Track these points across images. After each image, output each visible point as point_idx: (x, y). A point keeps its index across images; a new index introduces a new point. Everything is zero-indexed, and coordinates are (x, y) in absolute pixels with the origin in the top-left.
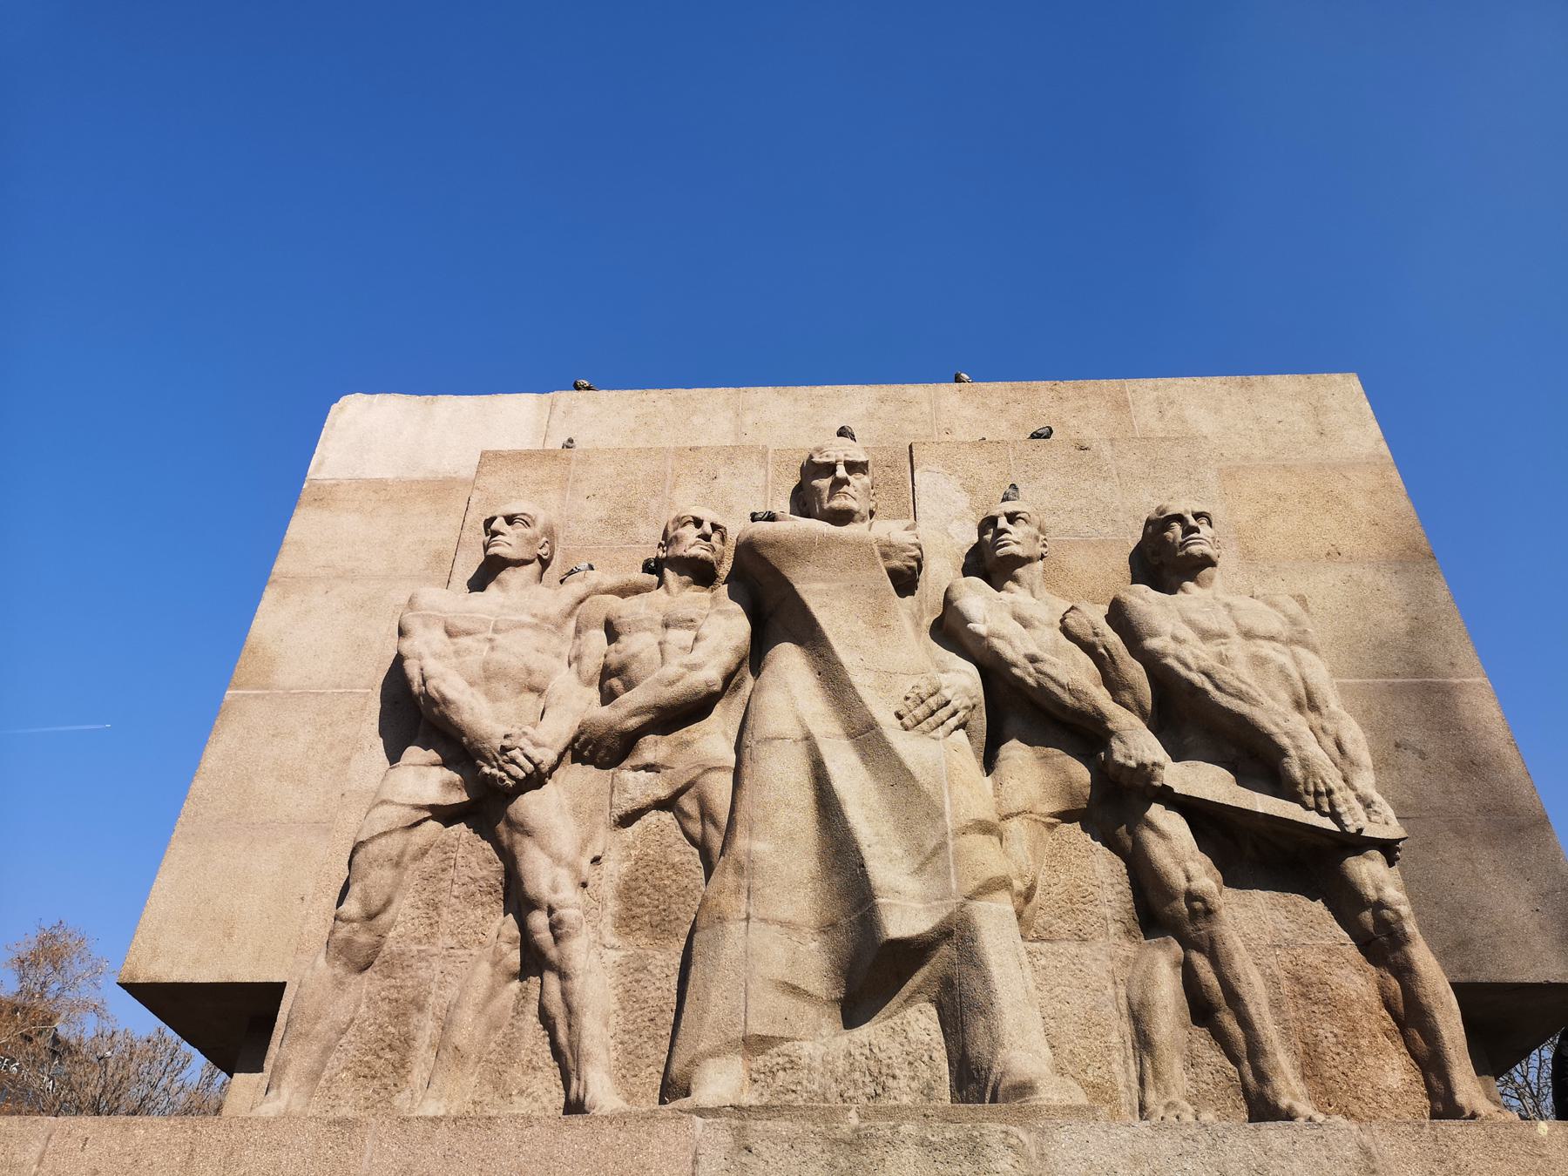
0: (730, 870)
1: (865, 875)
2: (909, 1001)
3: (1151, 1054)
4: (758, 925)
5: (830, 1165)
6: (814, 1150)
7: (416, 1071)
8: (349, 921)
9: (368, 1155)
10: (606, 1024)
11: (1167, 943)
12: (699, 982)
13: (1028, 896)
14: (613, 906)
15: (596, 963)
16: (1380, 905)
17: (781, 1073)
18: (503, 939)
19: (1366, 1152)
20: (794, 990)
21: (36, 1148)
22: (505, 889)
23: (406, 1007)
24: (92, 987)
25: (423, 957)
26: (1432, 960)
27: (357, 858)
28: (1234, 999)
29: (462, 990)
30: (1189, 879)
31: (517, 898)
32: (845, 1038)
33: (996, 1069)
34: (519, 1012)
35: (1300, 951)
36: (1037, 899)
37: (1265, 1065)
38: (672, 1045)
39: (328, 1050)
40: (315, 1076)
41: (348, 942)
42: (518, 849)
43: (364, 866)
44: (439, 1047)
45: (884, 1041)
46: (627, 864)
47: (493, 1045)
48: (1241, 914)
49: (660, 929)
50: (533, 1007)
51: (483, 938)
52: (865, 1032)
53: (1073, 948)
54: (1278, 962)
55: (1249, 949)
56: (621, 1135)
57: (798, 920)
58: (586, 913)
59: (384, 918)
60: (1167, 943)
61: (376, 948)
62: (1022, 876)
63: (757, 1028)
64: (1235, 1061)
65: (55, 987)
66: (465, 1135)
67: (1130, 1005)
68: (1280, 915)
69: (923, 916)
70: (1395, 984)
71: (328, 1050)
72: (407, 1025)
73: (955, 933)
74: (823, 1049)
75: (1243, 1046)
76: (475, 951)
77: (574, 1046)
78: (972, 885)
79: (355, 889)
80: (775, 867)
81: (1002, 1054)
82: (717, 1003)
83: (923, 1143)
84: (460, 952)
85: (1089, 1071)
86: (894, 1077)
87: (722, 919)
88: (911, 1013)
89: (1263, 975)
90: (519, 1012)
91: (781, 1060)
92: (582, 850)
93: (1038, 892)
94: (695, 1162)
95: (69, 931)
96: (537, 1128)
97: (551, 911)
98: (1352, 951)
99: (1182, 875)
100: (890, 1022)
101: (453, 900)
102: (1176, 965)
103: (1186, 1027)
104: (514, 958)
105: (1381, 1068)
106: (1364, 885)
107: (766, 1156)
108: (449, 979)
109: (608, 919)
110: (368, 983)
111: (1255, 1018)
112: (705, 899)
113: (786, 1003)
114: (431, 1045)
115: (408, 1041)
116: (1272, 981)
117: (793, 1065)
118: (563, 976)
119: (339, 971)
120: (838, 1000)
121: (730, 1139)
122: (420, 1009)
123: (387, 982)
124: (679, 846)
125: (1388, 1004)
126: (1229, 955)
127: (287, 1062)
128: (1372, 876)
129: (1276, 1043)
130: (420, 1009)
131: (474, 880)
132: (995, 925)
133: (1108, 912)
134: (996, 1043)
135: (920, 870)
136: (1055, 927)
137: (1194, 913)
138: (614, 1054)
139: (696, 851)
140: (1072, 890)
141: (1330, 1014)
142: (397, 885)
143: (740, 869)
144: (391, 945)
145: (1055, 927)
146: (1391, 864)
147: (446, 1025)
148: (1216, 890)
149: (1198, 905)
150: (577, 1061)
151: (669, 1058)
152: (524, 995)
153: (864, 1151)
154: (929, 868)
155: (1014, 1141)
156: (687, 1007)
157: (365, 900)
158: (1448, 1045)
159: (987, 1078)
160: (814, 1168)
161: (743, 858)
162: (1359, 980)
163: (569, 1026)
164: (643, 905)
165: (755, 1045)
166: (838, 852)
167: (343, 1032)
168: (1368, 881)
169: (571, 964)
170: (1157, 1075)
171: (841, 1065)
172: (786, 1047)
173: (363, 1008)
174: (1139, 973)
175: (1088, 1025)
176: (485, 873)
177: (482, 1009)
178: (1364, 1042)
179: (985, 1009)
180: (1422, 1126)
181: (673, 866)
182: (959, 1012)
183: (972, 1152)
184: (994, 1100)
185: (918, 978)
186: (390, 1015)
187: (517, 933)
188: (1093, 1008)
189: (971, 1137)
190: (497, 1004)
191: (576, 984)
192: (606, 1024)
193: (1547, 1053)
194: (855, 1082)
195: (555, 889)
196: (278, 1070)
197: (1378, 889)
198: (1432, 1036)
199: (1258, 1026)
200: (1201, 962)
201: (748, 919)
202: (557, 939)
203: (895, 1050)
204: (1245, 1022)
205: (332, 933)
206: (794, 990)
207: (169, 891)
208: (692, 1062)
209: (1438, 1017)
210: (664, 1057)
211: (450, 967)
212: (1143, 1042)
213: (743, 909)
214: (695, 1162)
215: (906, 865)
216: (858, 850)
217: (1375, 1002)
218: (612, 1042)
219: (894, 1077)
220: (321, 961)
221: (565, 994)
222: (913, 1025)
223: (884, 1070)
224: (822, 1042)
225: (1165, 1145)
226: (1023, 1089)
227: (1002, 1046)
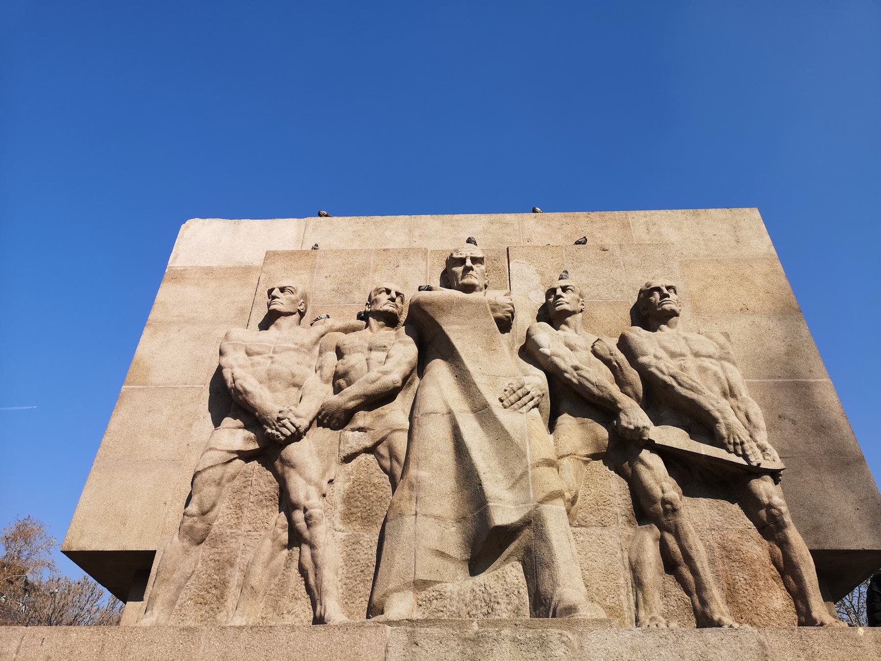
0: (406, 487)
1: (482, 490)
2: (506, 560)
3: (642, 590)
4: (421, 518)
5: (462, 653)
6: (453, 644)
7: (229, 601)
8: (192, 516)
9: (202, 648)
10: (337, 574)
11: (651, 528)
13: (573, 501)
14: (340, 507)
15: (331, 539)
16: (770, 506)
17: (435, 601)
18: (278, 526)
19: (762, 645)
20: (442, 554)
23: (224, 564)
25: (234, 536)
26: (799, 537)
27: (196, 480)
28: (689, 559)
29: (255, 555)
30: (663, 492)
31: (286, 503)
33: (555, 599)
34: (287, 567)
35: (725, 532)
36: (578, 503)
39: (180, 588)
40: (172, 603)
41: (191, 528)
42: (287, 475)
43: (200, 485)
44: (243, 587)
45: (492, 583)
46: (348, 484)
47: (273, 585)
48: (692, 511)
49: (367, 520)
50: (296, 564)
51: (267, 526)
52: (482, 578)
53: (598, 531)
54: (713, 539)
55: (697, 531)
56: (345, 636)
59: (212, 515)
61: (207, 531)
62: (570, 490)
63: (422, 575)
64: (689, 593)
65: (26, 553)
66: (257, 636)
68: (714, 512)
70: (778, 550)
71: (180, 588)
73: (532, 523)
76: (263, 533)
78: (541, 496)
79: (195, 498)
80: (431, 485)
81: (559, 590)
82: (400, 562)
83: (514, 640)
84: (254, 533)
85: (608, 599)
86: (498, 603)
87: (401, 515)
88: (508, 567)
89: (705, 545)
90: (287, 567)
91: (434, 594)
92: (323, 476)
93: (579, 499)
94: (387, 651)
96: (297, 632)
97: (305, 510)
98: (754, 532)
100: (496, 573)
101: (250, 504)
102: (656, 540)
103: (661, 574)
104: (285, 536)
107: (426, 647)
108: (248, 548)
110: (202, 551)
111: (700, 570)
112: (392, 503)
113: (438, 562)
114: (238, 586)
115: (225, 583)
116: (710, 549)
117: (441, 596)
118: (312, 547)
120: (466, 560)
121: (406, 638)
122: (232, 565)
123: (213, 550)
124: (377, 474)
125: (774, 562)
126: (686, 534)
127: (156, 595)
128: (766, 490)
129: (712, 584)
130: (232, 565)
131: (262, 493)
132: (555, 519)
133: (618, 510)
134: (555, 584)
137: (666, 511)
138: (341, 591)
140: (598, 498)
142: (219, 495)
143: (411, 486)
144: (215, 529)
146: (776, 483)
147: (246, 574)
148: (678, 498)
149: (668, 506)
152: (290, 558)
153: (481, 645)
155: (565, 639)
156: (382, 564)
157: (201, 504)
158: (808, 584)
159: (550, 604)
160: (453, 654)
161: (414, 481)
162: (759, 549)
163: (316, 575)
164: (357, 507)
165: (420, 585)
166: (467, 477)
167: (188, 578)
168: (764, 493)
169: (317, 540)
170: (645, 601)
174: (636, 544)
175: (607, 574)
176: (268, 489)
177: (267, 565)
178: (761, 583)
179: (549, 565)
180: (793, 630)
181: (374, 485)
182: (535, 567)
183: (542, 645)
184: (554, 616)
185: (512, 548)
186: (215, 569)
188: (610, 564)
189: (541, 637)
190: (275, 562)
191: (320, 551)
193: (864, 589)
194: (476, 606)
195: (307, 498)
196: (152, 600)
197: (769, 497)
198: (799, 579)
199: (702, 574)
200: (670, 538)
201: (416, 514)
202: (309, 526)
203: (499, 588)
204: (695, 572)
205: (182, 522)
206: (442, 554)
209: (803, 569)
210: (369, 592)
211: (248, 542)
212: (638, 583)
213: (413, 508)
214: (387, 651)
215: (505, 484)
216: (478, 476)
217: (767, 560)
219: (498, 603)
220: (176, 538)
221: (313, 557)
222: (509, 574)
223: (493, 599)
224: (458, 584)
225: (650, 641)
226: (570, 610)
227: (559, 585)
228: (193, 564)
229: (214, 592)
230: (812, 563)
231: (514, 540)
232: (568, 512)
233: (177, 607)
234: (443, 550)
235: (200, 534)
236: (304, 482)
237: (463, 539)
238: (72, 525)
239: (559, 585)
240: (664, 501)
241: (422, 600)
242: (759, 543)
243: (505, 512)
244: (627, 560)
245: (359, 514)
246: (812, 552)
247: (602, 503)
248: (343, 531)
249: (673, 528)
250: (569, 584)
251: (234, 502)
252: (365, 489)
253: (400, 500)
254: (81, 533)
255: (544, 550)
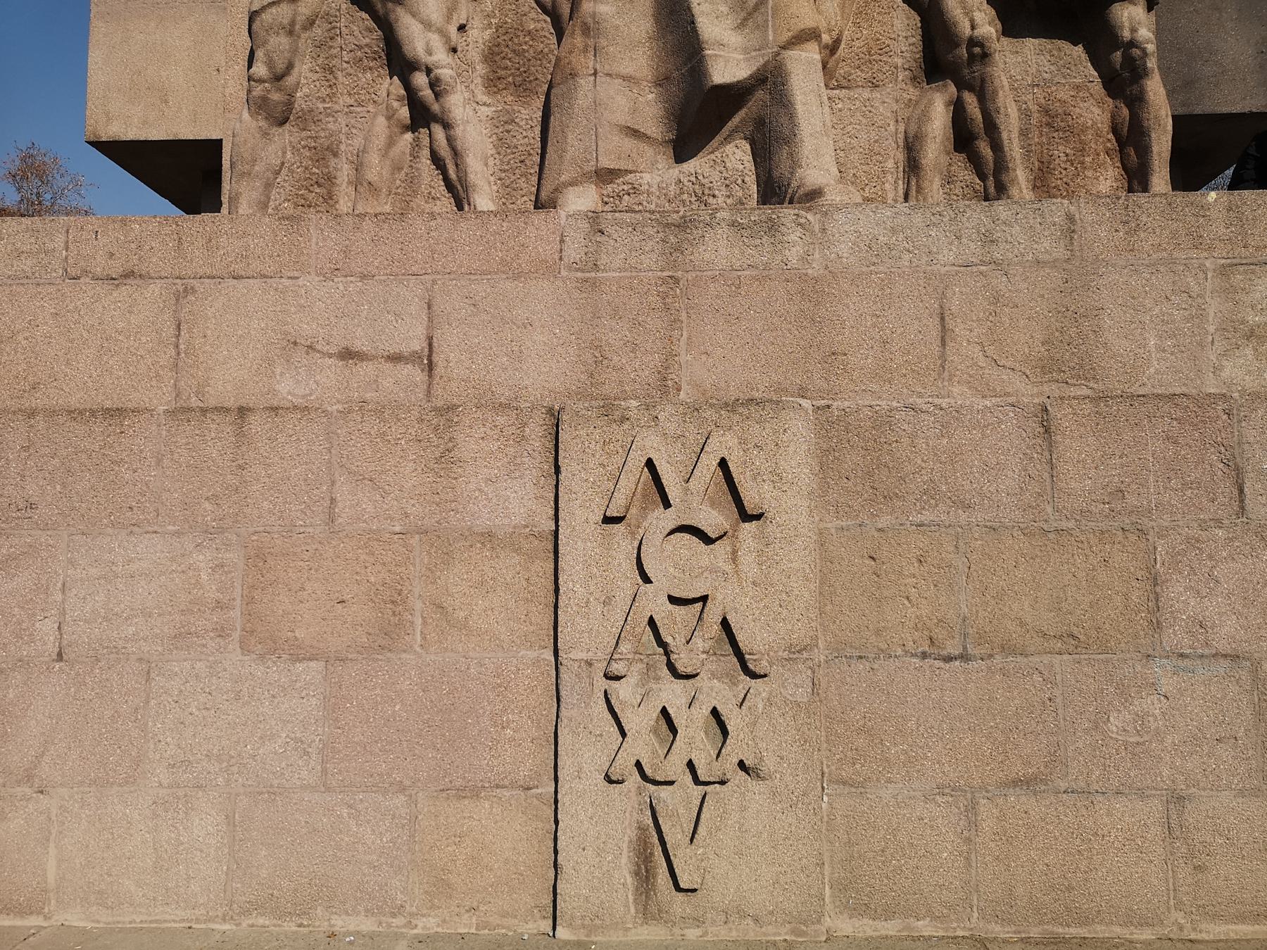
0: (578, 32)
1: (695, 31)
2: (728, 139)
3: (918, 176)
4: (603, 79)
6: (651, 231)
7: (341, 202)
8: (261, 81)
10: (486, 165)
11: (945, 86)
13: (833, 48)
14: (481, 69)
15: (472, 115)
16: (1132, 44)
17: (626, 197)
18: (392, 97)
19: (1070, 218)
20: (635, 133)
23: (325, 153)
25: (330, 113)
26: (1162, 91)
27: (254, 27)
28: (991, 128)
29: (366, 139)
30: (973, 28)
31: (399, 62)
33: (794, 184)
34: (415, 157)
35: (1054, 88)
36: (841, 52)
39: (268, 186)
40: (264, 206)
41: (264, 99)
42: (392, 17)
43: (263, 33)
44: (357, 183)
45: (707, 171)
46: (488, 32)
47: (398, 182)
48: (1011, 59)
49: (522, 88)
50: (426, 152)
51: (376, 98)
52: (691, 165)
53: (866, 94)
54: (1032, 100)
55: (1013, 89)
59: (290, 80)
61: (289, 105)
62: (830, 31)
63: (606, 162)
64: (982, 176)
65: (48, 196)
68: (1043, 60)
70: (1125, 112)
71: (268, 186)
73: (770, 80)
76: (371, 108)
78: (786, 36)
79: (260, 54)
80: (617, 27)
81: (799, 172)
82: (574, 146)
83: (733, 224)
84: (359, 109)
85: (867, 189)
86: (714, 196)
87: (573, 75)
88: (729, 148)
89: (1019, 110)
90: (415, 157)
91: (626, 187)
92: (449, 18)
93: (843, 46)
94: (562, 241)
96: (439, 220)
97: (429, 71)
98: (1097, 87)
100: (712, 156)
101: (345, 65)
102: (948, 104)
103: (948, 154)
104: (404, 112)
108: (354, 131)
110: (286, 136)
111: (1006, 142)
112: (558, 59)
113: (629, 143)
114: (350, 183)
115: (330, 179)
116: (1025, 114)
117: (635, 190)
118: (447, 126)
120: (671, 141)
121: (587, 225)
122: (335, 155)
123: (304, 134)
124: (533, 15)
125: (1115, 130)
126: (995, 92)
127: (238, 195)
128: (1130, 19)
129: (1018, 162)
130: (335, 155)
131: (360, 47)
132: (803, 72)
133: (899, 61)
134: (795, 164)
137: (972, 57)
138: (495, 188)
140: (872, 43)
142: (294, 51)
143: (586, 31)
144: (300, 103)
146: (1150, 9)
147: (358, 167)
148: (994, 35)
149: (977, 50)
152: (417, 144)
155: (803, 221)
156: (550, 149)
157: (270, 64)
158: (1155, 157)
159: (786, 192)
161: (589, 20)
162: (1097, 111)
163: (457, 165)
164: (506, 68)
165: (605, 176)
166: (672, 12)
167: (278, 173)
168: (1126, 24)
169: (452, 115)
170: (919, 189)
174: (918, 112)
175: (871, 154)
176: (367, 40)
177: (385, 153)
178: (1088, 159)
179: (790, 139)
180: (1118, 198)
181: (529, 32)
182: (769, 145)
184: (791, 202)
185: (736, 120)
186: (311, 159)
188: (876, 141)
189: (770, 219)
190: (396, 151)
191: (458, 131)
193: (1232, 169)
194: (683, 201)
195: (429, 52)
196: (234, 200)
197: (1134, 30)
198: (1144, 151)
199: (1006, 149)
200: (970, 100)
201: (595, 74)
202: (437, 95)
203: (716, 176)
204: (997, 147)
205: (249, 91)
206: (635, 133)
209: (1153, 135)
210: (534, 189)
211: (353, 121)
212: (913, 166)
213: (591, 64)
214: (562, 241)
215: (730, 22)
216: (689, 9)
217: (1105, 127)
219: (714, 196)
220: (246, 115)
221: (450, 140)
222: (733, 157)
223: (707, 192)
224: (658, 174)
225: (918, 219)
226: (814, 195)
227: (800, 166)
228: (280, 153)
229: (318, 190)
230: (1170, 128)
231: (740, 108)
232: (824, 67)
233: (270, 210)
234: (636, 127)
235: (279, 109)
236: (420, 26)
237: (666, 109)
238: (89, 104)
239: (800, 166)
240: (972, 42)
241: (608, 196)
242: (1100, 103)
243: (728, 66)
244: (901, 136)
245: (510, 79)
246: (1173, 116)
247: (876, 51)
248: (489, 105)
249: (978, 83)
250: (816, 158)
251: (319, 62)
252: (516, 40)
253: (571, 52)
254: (107, 116)
255: (784, 120)
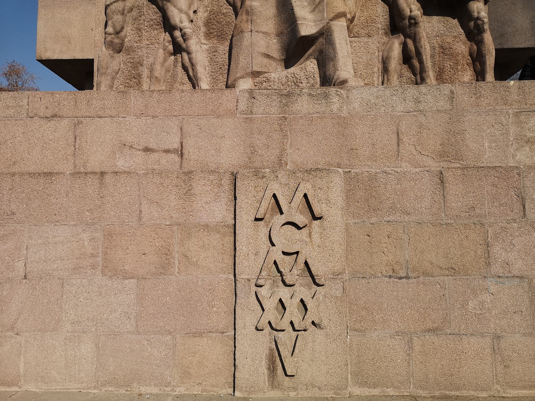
0: (244, 13)
1: (293, 13)
2: (307, 59)
3: (387, 74)
4: (255, 33)
6: (275, 98)
7: (144, 85)
8: (110, 34)
10: (205, 69)
11: (399, 36)
12: (236, 54)
13: (352, 20)
14: (203, 29)
15: (199, 48)
16: (478, 18)
17: (264, 83)
18: (165, 41)
19: (452, 92)
20: (268, 56)
21: (25, 101)
22: (163, 23)
23: (137, 64)
24: (33, 84)
25: (139, 48)
26: (491, 38)
27: (107, 11)
28: (419, 54)
29: (154, 59)
30: (411, 12)
31: (168, 26)
32: (286, 72)
33: (335, 78)
34: (175, 66)
35: (445, 37)
36: (355, 22)
37: (424, 75)
38: (228, 76)
39: (113, 78)
40: (111, 87)
41: (112, 42)
42: (166, 7)
43: (111, 14)
44: (151, 77)
45: (298, 72)
46: (206, 13)
47: (168, 77)
48: (427, 25)
49: (221, 37)
50: (180, 64)
51: (159, 41)
52: (292, 70)
53: (366, 40)
54: (436, 42)
55: (428, 37)
57: (269, 32)
58: (194, 32)
59: (122, 34)
60: (399, 36)
61: (122, 44)
62: (350, 13)
63: (256, 69)
64: (415, 74)
65: (20, 83)
67: (383, 58)
68: (441, 25)
69: (314, 27)
70: (475, 47)
71: (113, 78)
72: (138, 70)
73: (325, 34)
74: (278, 76)
75: (419, 70)
76: (157, 46)
77: (195, 76)
78: (332, 15)
79: (110, 23)
80: (261, 12)
81: (337, 73)
82: (242, 61)
83: (309, 95)
84: (151, 46)
85: (366, 80)
86: (301, 83)
87: (242, 32)
88: (308, 63)
89: (430, 46)
90: (175, 66)
91: (264, 79)
92: (189, 8)
93: (356, 19)
94: (237, 102)
95: (18, 64)
96: (186, 93)
97: (181, 30)
98: (463, 37)
99: (409, 10)
100: (301, 66)
101: (146, 27)
102: (400, 44)
103: (400, 65)
104: (171, 47)
105: (463, 75)
106: (474, 12)
108: (150, 55)
109: (202, 34)
110: (121, 57)
111: (425, 60)
112: (236, 25)
113: (266, 61)
114: (148, 77)
115: (140, 75)
116: (433, 48)
117: (268, 80)
118: (189, 53)
119: (111, 52)
120: (283, 59)
121: (248, 95)
122: (142, 65)
123: (128, 56)
124: (225, 6)
125: (471, 55)
126: (420, 39)
127: (101, 82)
128: (477, 8)
129: (430, 68)
130: (142, 65)
131: (152, 20)
132: (339, 30)
133: (380, 26)
134: (336, 69)
135: (313, 11)
136: (360, 32)
137: (410, 24)
138: (209, 79)
139: (232, 8)
140: (368, 18)
141: (450, 59)
142: (124, 21)
143: (248, 13)
144: (127, 43)
145: (360, 32)
146: (485, 4)
147: (151, 71)
148: (420, 15)
149: (413, 21)
150: (197, 81)
151: (227, 80)
152: (176, 61)
154: (317, 10)
155: (339, 93)
156: (232, 63)
157: (114, 27)
158: (488, 66)
159: (332, 81)
161: (249, 8)
162: (463, 47)
163: (193, 70)
164: (214, 29)
165: (255, 74)
166: (284, 5)
167: (117, 73)
168: (476, 10)
169: (191, 49)
170: (388, 80)
171: (284, 80)
172: (266, 75)
173: (122, 65)
174: (388, 47)
175: (368, 65)
176: (155, 17)
177: (162, 65)
178: (459, 67)
179: (333, 59)
180: (472, 84)
181: (224, 14)
182: (325, 61)
184: (334, 85)
185: (311, 51)
186: (131, 67)
187: (170, 39)
188: (370, 60)
189: (325, 93)
190: (167, 64)
191: (193, 56)
192: (205, 69)
193: (520, 71)
194: (289, 85)
195: (181, 22)
196: (99, 84)
197: (479, 13)
198: (483, 64)
199: (425, 63)
200: (410, 42)
201: (251, 31)
202: (185, 40)
203: (302, 74)
204: (421, 62)
205: (105, 39)
206: (268, 56)
207: (43, 28)
208: (235, 80)
209: (487, 57)
210: (225, 80)
211: (149, 51)
212: (385, 70)
213: (250, 27)
214: (237, 102)
215: (308, 9)
216: (291, 4)
217: (467, 54)
218: (208, 75)
219: (301, 83)
220: (104, 49)
221: (190, 59)
222: (310, 66)
223: (298, 81)
224: (278, 73)
225: (388, 92)
226: (344, 82)
227: (338, 70)
228: (118, 65)
229: (134, 80)
230: (494, 54)
231: (312, 46)
232: (348, 28)
233: (114, 89)
234: (269, 54)
235: (118, 46)
236: (177, 11)
237: (281, 46)
238: (38, 44)
239: (338, 70)
240: (411, 18)
241: (257, 83)
242: (464, 44)
243: (307, 28)
244: (381, 57)
245: (215, 33)
246: (495, 49)
247: (370, 22)
248: (206, 44)
249: (413, 35)
250: (345, 67)
251: (135, 26)
252: (218, 17)
253: (241, 22)
254: (45, 49)
255: (331, 51)
